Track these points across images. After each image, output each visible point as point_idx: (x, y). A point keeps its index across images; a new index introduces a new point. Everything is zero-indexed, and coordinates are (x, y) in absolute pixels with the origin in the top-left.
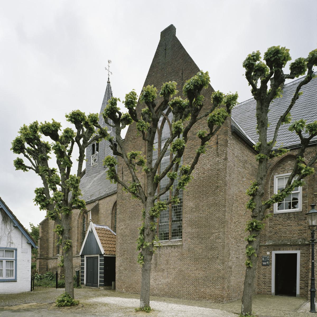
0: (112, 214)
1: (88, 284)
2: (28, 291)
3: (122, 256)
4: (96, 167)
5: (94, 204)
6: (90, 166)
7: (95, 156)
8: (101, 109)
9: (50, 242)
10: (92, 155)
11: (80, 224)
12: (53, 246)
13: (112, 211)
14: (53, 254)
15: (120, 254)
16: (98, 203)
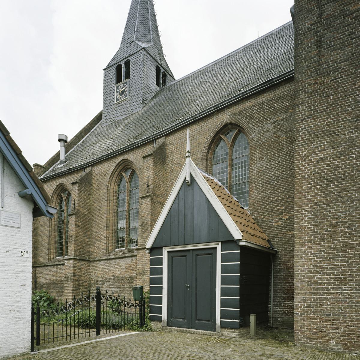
0: (207, 160)
1: (172, 319)
2: (21, 351)
3: (323, 239)
4: (125, 104)
5: (155, 145)
6: (111, 104)
7: (122, 85)
8: (131, 7)
9: (40, 234)
10: (115, 84)
11: (112, 194)
12: (47, 241)
13: (208, 153)
14: (48, 257)
15: (315, 234)
16: (165, 142)
